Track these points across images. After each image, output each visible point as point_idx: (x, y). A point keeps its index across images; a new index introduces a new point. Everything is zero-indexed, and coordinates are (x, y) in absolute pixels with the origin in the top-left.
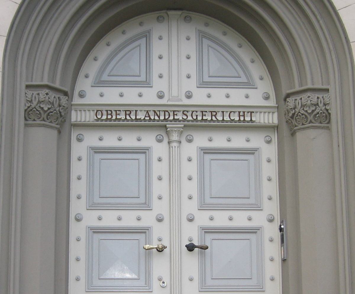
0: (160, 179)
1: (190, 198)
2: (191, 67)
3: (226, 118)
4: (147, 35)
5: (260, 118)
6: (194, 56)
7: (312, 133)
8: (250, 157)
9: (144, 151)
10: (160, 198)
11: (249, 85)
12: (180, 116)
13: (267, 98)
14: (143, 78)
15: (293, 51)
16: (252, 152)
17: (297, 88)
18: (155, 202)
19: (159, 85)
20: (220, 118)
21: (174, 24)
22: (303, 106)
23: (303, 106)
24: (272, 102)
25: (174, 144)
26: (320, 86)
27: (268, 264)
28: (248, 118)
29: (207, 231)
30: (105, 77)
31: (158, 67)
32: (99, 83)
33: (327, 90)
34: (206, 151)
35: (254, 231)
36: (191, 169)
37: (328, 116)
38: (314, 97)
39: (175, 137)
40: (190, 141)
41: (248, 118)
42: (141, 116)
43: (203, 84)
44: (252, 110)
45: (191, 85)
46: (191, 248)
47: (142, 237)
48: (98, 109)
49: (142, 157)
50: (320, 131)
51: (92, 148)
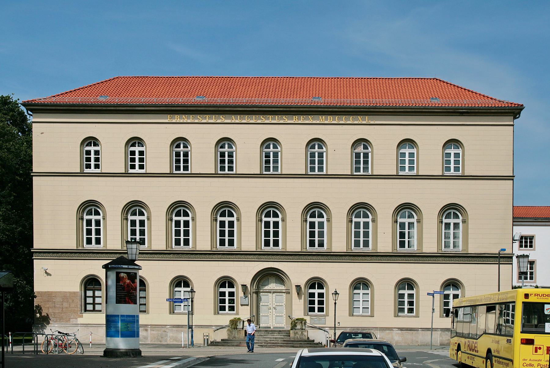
16: (268, 295)
30: (263, 285)
34: (276, 295)
35: (282, 316)
37: (289, 293)
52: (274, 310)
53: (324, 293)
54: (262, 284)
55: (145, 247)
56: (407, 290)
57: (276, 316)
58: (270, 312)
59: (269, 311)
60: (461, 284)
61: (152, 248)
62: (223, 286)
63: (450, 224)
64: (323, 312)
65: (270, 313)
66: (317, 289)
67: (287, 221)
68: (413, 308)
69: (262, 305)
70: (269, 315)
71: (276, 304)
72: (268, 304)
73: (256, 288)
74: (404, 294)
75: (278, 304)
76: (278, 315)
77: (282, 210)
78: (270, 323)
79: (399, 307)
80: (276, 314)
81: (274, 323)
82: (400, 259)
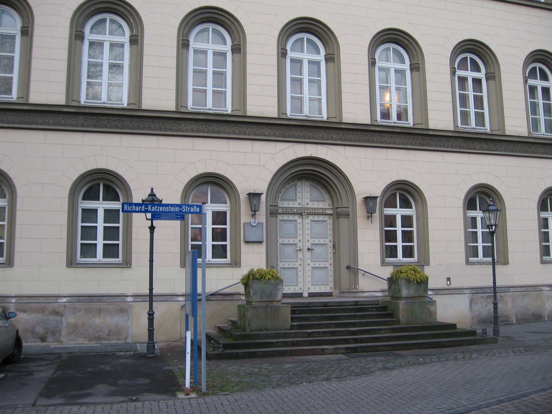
0: (300, 235)
1: (308, 235)
2: (308, 195)
3: (319, 212)
4: (296, 185)
5: (329, 212)
6: (309, 192)
7: (344, 219)
8: (325, 246)
9: (295, 221)
10: (300, 235)
11: (324, 201)
12: (306, 211)
13: (329, 205)
14: (294, 198)
15: (340, 199)
16: (325, 221)
17: (340, 206)
18: (299, 236)
19: (299, 201)
20: (317, 212)
21: (303, 182)
22: (342, 212)
23: (342, 212)
24: (331, 207)
25: (304, 219)
26: (346, 206)
27: (329, 254)
28: (325, 212)
29: (313, 244)
30: (284, 198)
31: (299, 195)
32: (282, 200)
33: (349, 207)
34: (312, 221)
35: (326, 268)
36: (309, 273)
37: (348, 215)
38: (345, 209)
39: (304, 217)
40: (308, 218)
41: (325, 212)
42: (295, 211)
43: (311, 201)
44: (326, 209)
45: (308, 201)
46: (308, 249)
47: (295, 246)
48: (283, 208)
49: (295, 270)
50: (346, 219)
51: (281, 244)
52: (308, 254)
53: (226, 212)
54: (283, 195)
55: (12, 98)
56: (104, 200)
57: (313, 268)
58: (299, 260)
59: (297, 257)
60: (417, 192)
61: (507, 128)
62: (91, 195)
63: (205, 52)
64: (118, 257)
65: (300, 262)
66: (400, 208)
67: (146, 42)
68: (226, 245)
69: (282, 244)
70: (297, 265)
71: (312, 241)
72: (297, 241)
73: (272, 203)
74: (96, 211)
75: (317, 241)
76: (317, 265)
77: (320, 30)
78: (301, 285)
79: (200, 243)
80: (312, 265)
81: (309, 285)
82: (353, 138)
